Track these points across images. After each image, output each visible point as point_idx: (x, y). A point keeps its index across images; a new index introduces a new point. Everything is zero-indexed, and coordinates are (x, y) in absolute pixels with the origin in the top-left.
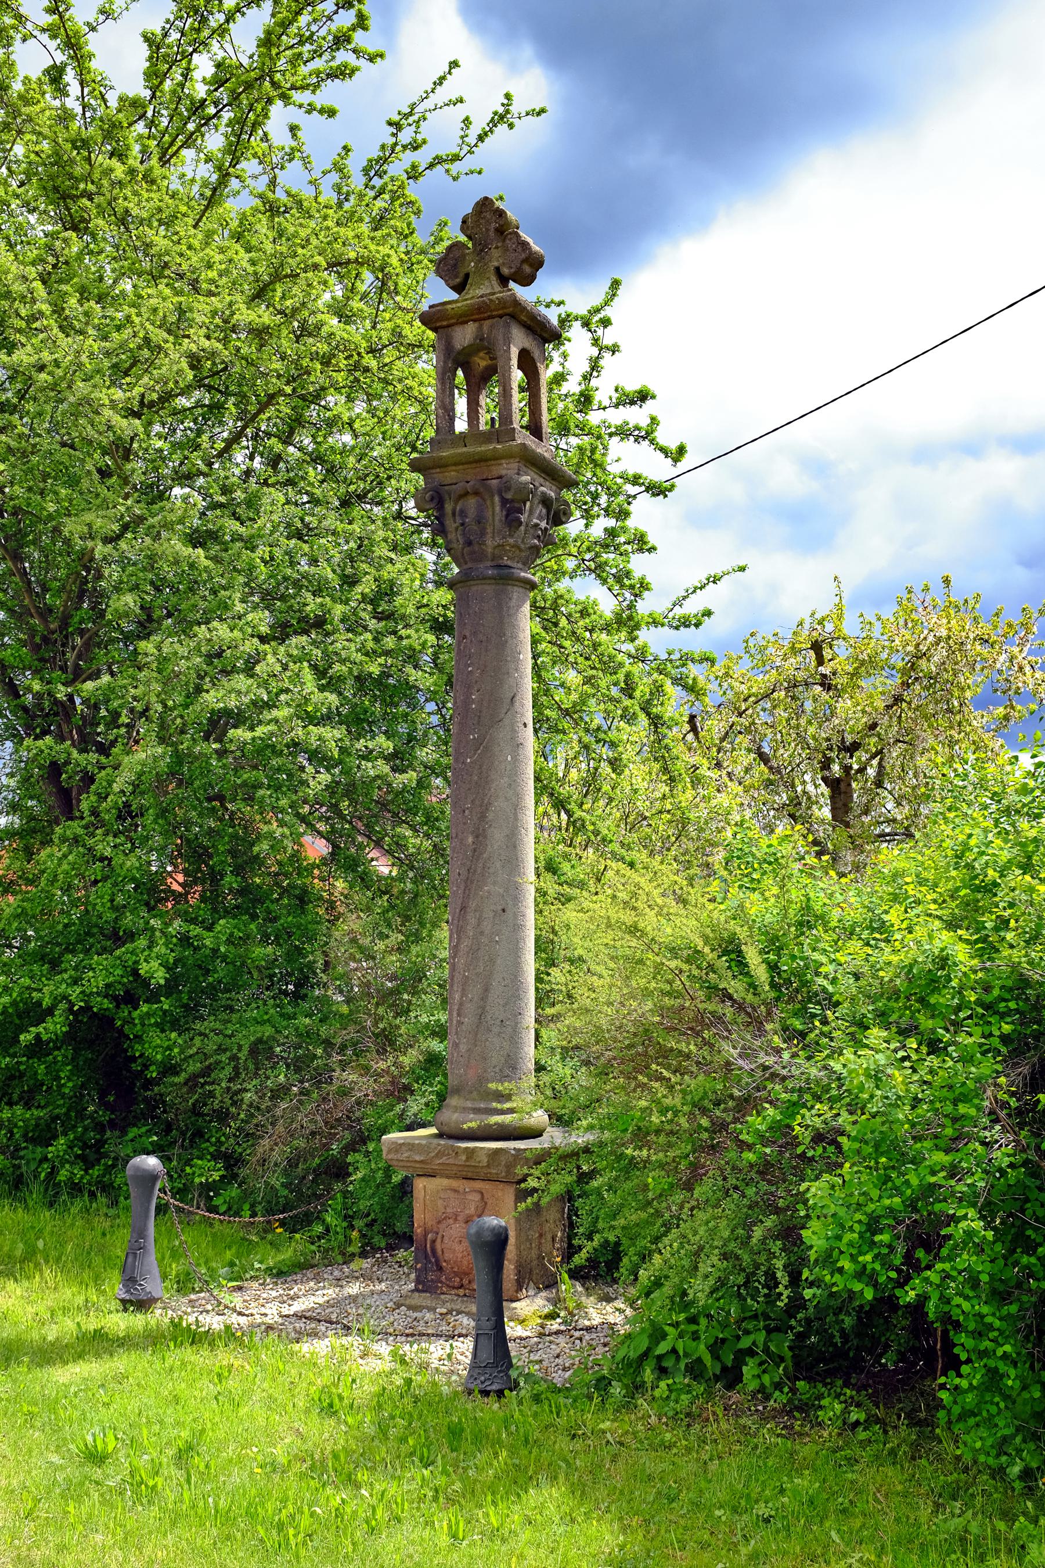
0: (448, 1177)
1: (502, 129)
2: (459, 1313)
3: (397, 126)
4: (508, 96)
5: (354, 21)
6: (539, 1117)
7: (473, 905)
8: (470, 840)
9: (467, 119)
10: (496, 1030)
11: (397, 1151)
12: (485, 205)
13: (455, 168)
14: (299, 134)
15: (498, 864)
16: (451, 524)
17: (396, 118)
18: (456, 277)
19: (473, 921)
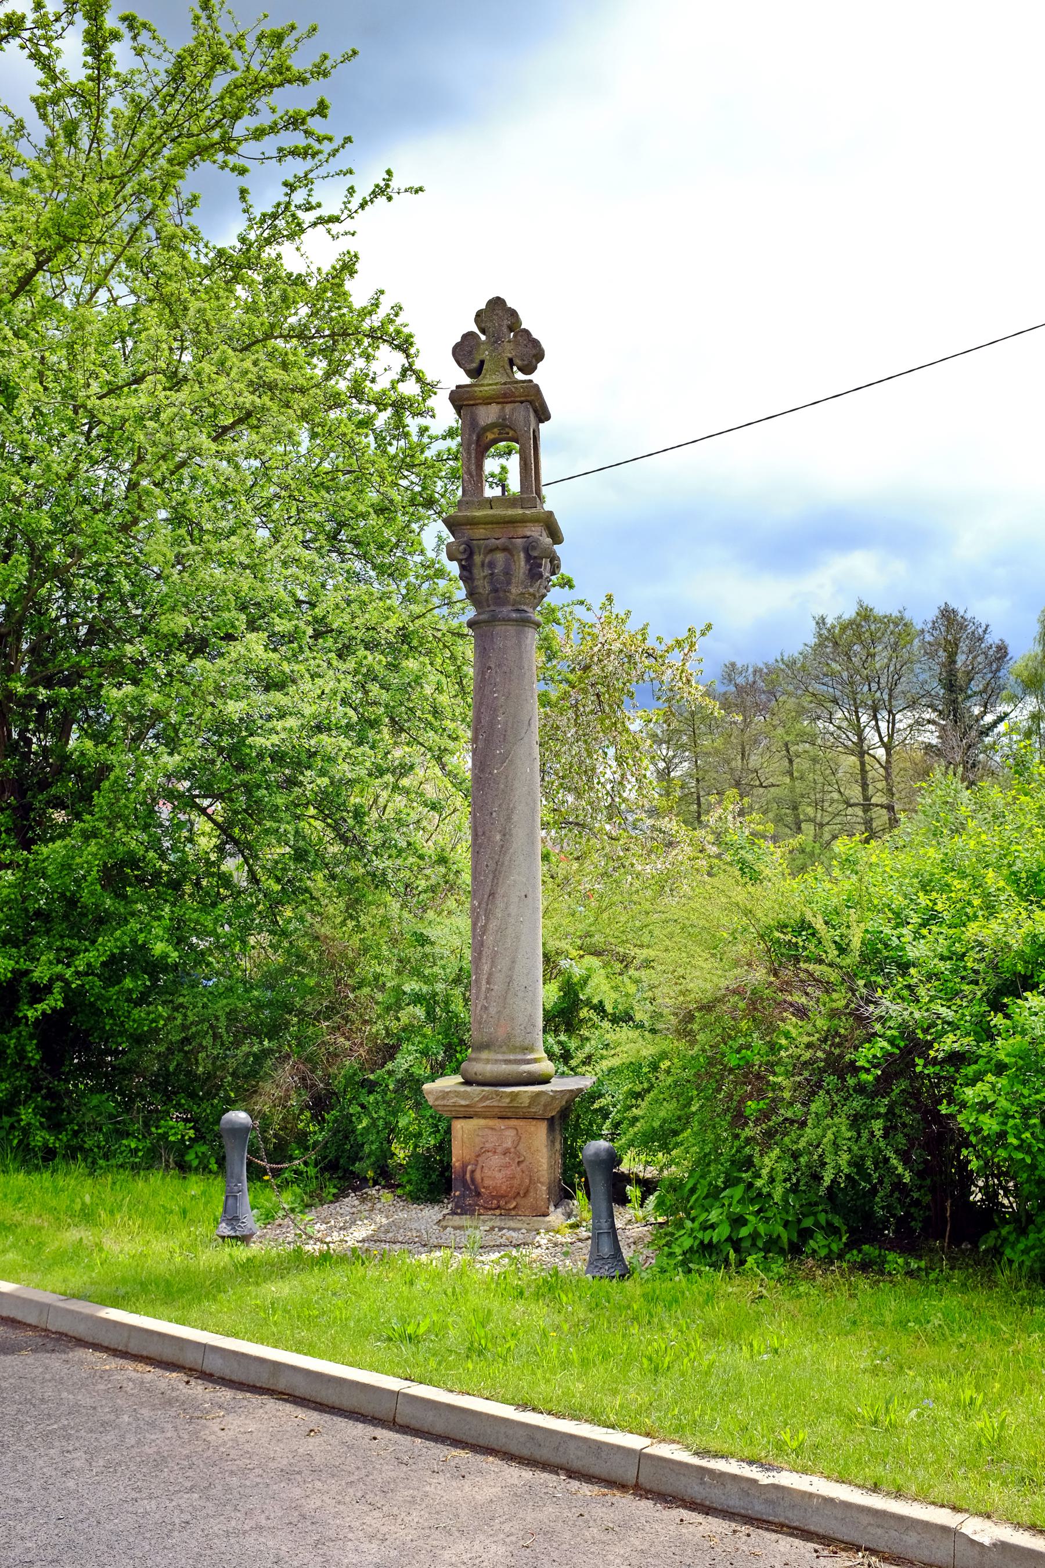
0: (485, 1118)
1: (381, 200)
2: (501, 1229)
3: (291, 187)
4: (389, 172)
5: (315, 107)
6: (546, 1066)
7: (501, 891)
8: (498, 837)
9: (352, 188)
10: (520, 994)
11: (444, 1098)
12: (497, 303)
13: (335, 227)
14: (248, 197)
15: (522, 858)
16: (480, 573)
17: (291, 180)
18: (472, 361)
19: (502, 905)
